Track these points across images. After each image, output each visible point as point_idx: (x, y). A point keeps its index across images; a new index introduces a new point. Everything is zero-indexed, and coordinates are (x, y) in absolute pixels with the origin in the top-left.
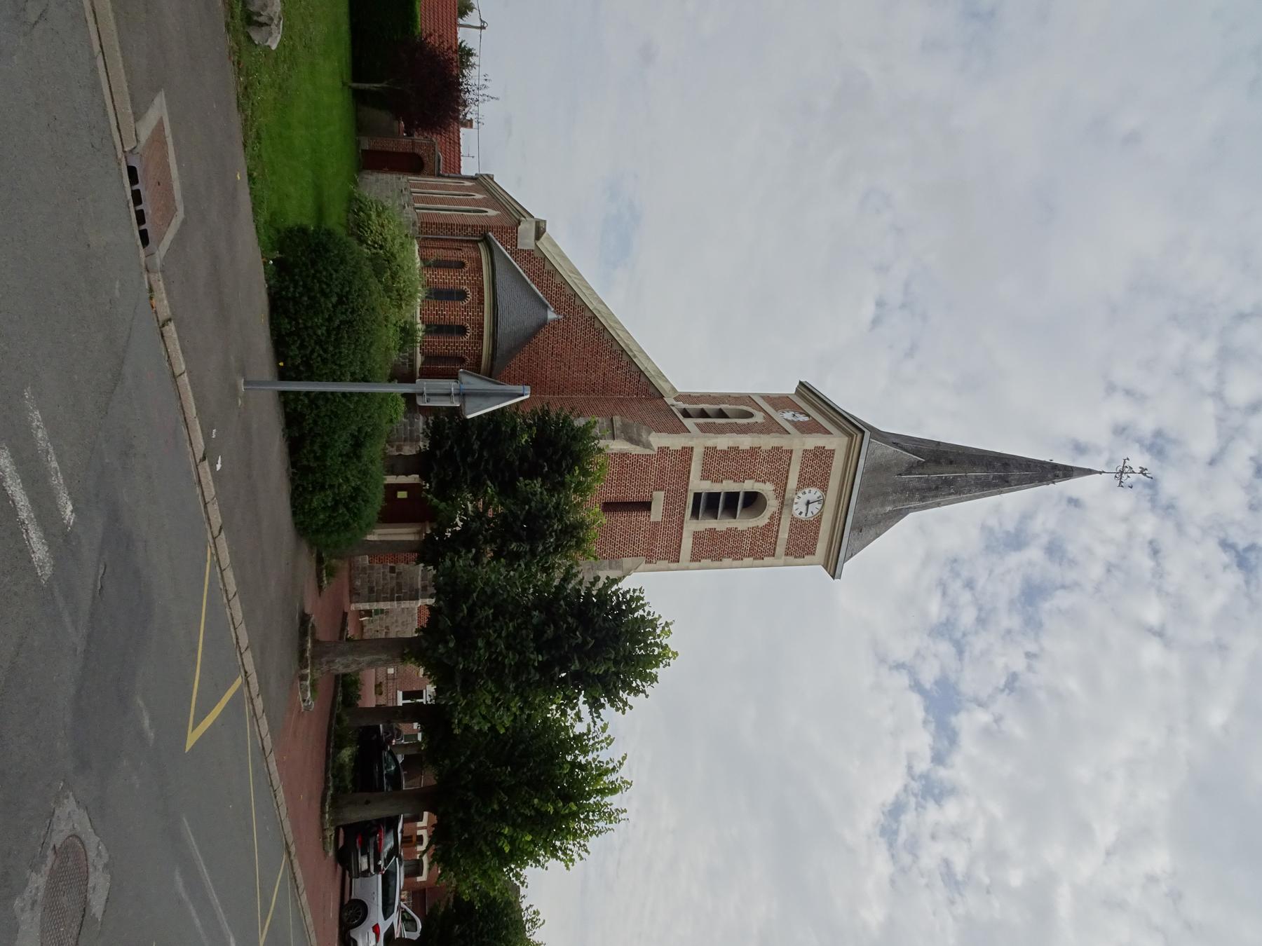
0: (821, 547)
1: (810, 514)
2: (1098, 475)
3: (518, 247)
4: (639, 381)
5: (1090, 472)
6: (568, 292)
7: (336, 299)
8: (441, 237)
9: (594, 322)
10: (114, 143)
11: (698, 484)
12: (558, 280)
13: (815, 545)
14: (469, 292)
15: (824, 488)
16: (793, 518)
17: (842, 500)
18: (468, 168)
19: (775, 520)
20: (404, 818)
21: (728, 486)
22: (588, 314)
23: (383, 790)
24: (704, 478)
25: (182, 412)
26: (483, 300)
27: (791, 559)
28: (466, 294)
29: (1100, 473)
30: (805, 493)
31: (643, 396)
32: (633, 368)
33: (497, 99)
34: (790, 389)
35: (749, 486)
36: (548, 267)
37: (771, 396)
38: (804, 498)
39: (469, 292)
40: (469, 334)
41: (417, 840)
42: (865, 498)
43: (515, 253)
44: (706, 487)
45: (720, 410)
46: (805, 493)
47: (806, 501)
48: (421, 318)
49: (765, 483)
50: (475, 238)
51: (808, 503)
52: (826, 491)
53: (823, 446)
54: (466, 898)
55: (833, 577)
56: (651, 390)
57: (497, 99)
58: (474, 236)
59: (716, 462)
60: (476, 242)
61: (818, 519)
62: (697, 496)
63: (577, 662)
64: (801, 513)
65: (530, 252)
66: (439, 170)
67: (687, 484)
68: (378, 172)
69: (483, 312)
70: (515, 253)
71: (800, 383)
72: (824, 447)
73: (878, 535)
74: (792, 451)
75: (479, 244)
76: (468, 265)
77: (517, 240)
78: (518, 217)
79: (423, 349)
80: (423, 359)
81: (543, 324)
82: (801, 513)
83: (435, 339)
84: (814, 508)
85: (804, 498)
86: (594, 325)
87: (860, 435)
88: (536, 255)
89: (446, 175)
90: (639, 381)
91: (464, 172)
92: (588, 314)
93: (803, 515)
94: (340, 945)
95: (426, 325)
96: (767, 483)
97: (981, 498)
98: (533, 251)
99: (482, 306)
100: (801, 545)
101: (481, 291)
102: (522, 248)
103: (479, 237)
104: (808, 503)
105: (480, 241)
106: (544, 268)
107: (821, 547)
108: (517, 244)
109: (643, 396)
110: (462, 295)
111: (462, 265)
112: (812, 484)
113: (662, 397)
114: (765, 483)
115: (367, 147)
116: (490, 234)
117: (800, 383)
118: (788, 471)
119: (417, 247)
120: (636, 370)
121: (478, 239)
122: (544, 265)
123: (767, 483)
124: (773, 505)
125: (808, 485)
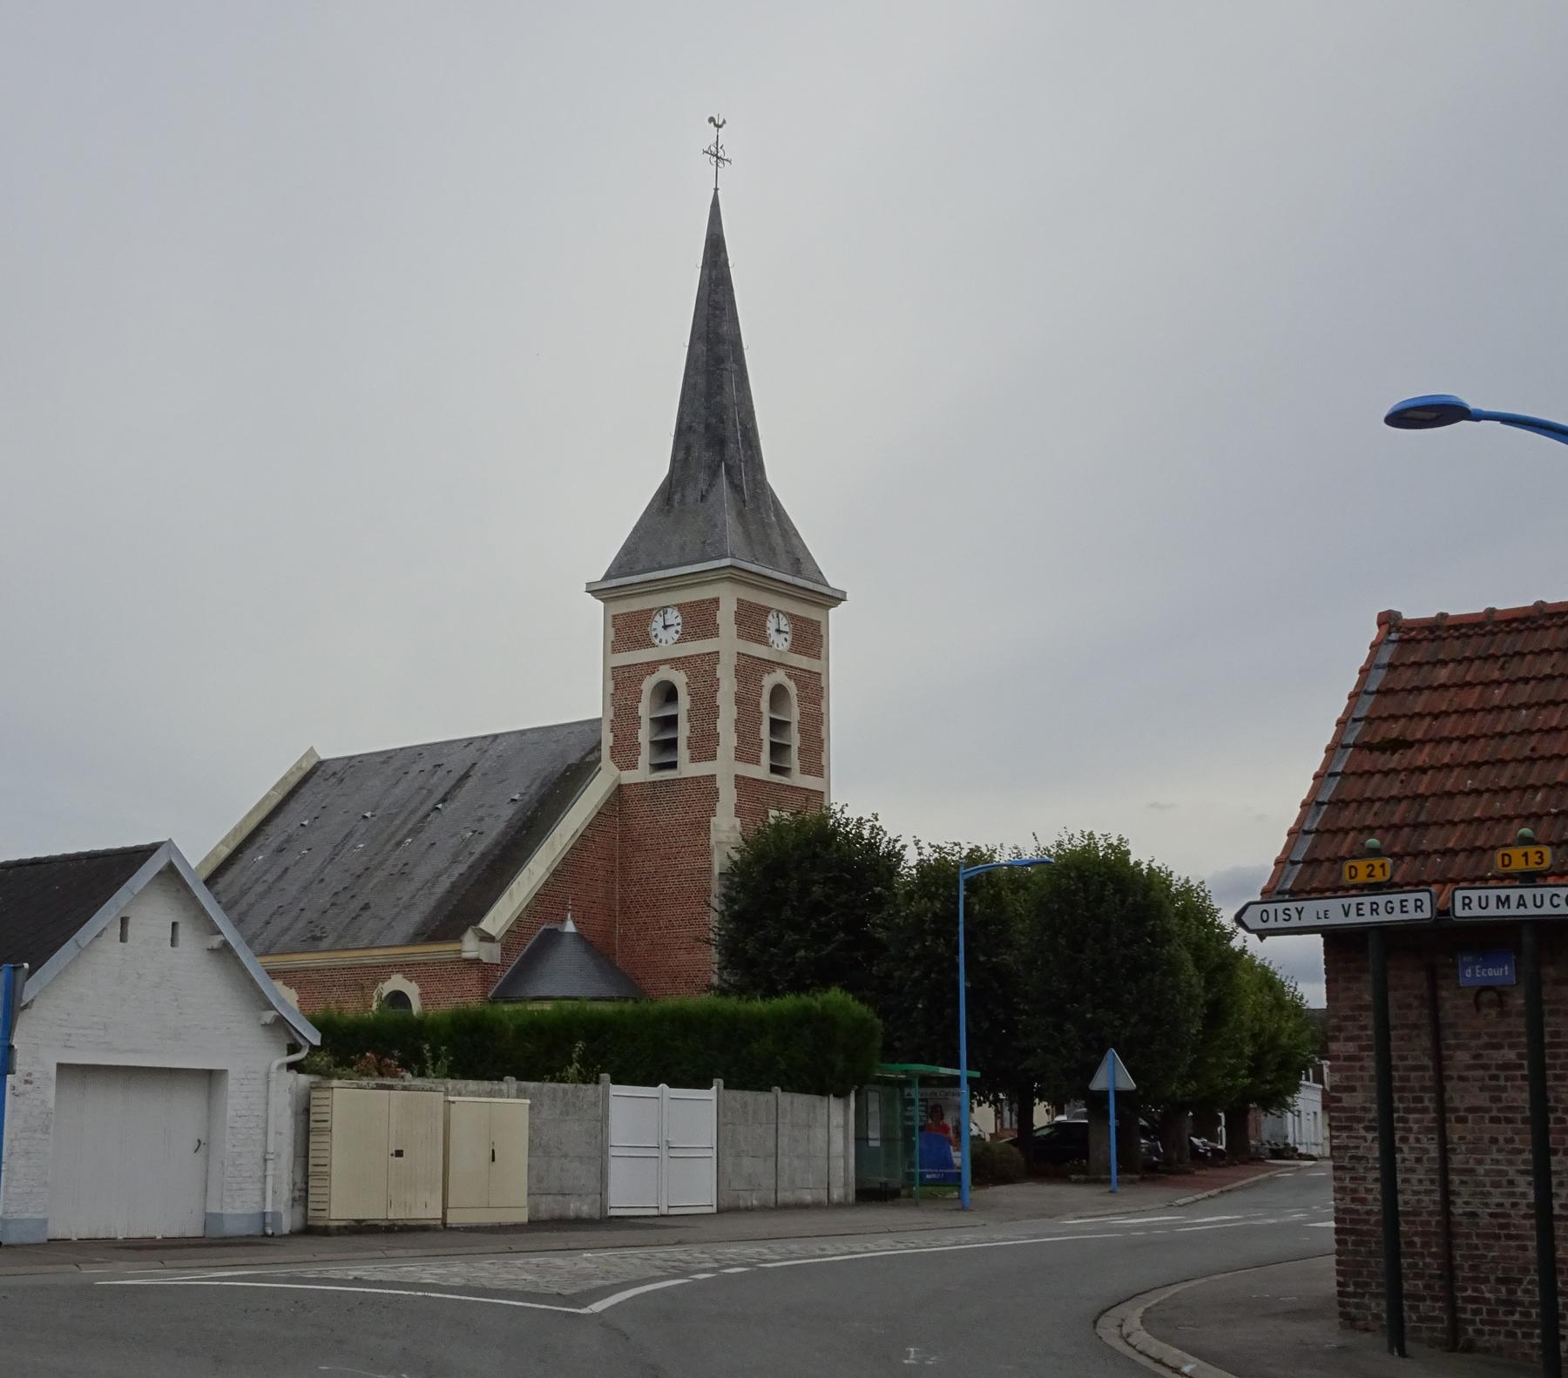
0: (811, 613)
3: (499, 962)
15: (767, 610)
16: (679, 641)
17: (780, 590)
19: (676, 663)
20: (1272, 1159)
24: (758, 762)
29: (716, 189)
42: (771, 558)
44: (645, 756)
51: (778, 631)
54: (676, 637)
59: (746, 753)
61: (792, 618)
63: (1470, 1275)
67: (763, 781)
73: (797, 534)
74: (738, 653)
81: (579, 936)
88: (505, 941)
93: (787, 637)
94: (8, 866)
100: (810, 638)
107: (811, 613)
124: (779, 676)
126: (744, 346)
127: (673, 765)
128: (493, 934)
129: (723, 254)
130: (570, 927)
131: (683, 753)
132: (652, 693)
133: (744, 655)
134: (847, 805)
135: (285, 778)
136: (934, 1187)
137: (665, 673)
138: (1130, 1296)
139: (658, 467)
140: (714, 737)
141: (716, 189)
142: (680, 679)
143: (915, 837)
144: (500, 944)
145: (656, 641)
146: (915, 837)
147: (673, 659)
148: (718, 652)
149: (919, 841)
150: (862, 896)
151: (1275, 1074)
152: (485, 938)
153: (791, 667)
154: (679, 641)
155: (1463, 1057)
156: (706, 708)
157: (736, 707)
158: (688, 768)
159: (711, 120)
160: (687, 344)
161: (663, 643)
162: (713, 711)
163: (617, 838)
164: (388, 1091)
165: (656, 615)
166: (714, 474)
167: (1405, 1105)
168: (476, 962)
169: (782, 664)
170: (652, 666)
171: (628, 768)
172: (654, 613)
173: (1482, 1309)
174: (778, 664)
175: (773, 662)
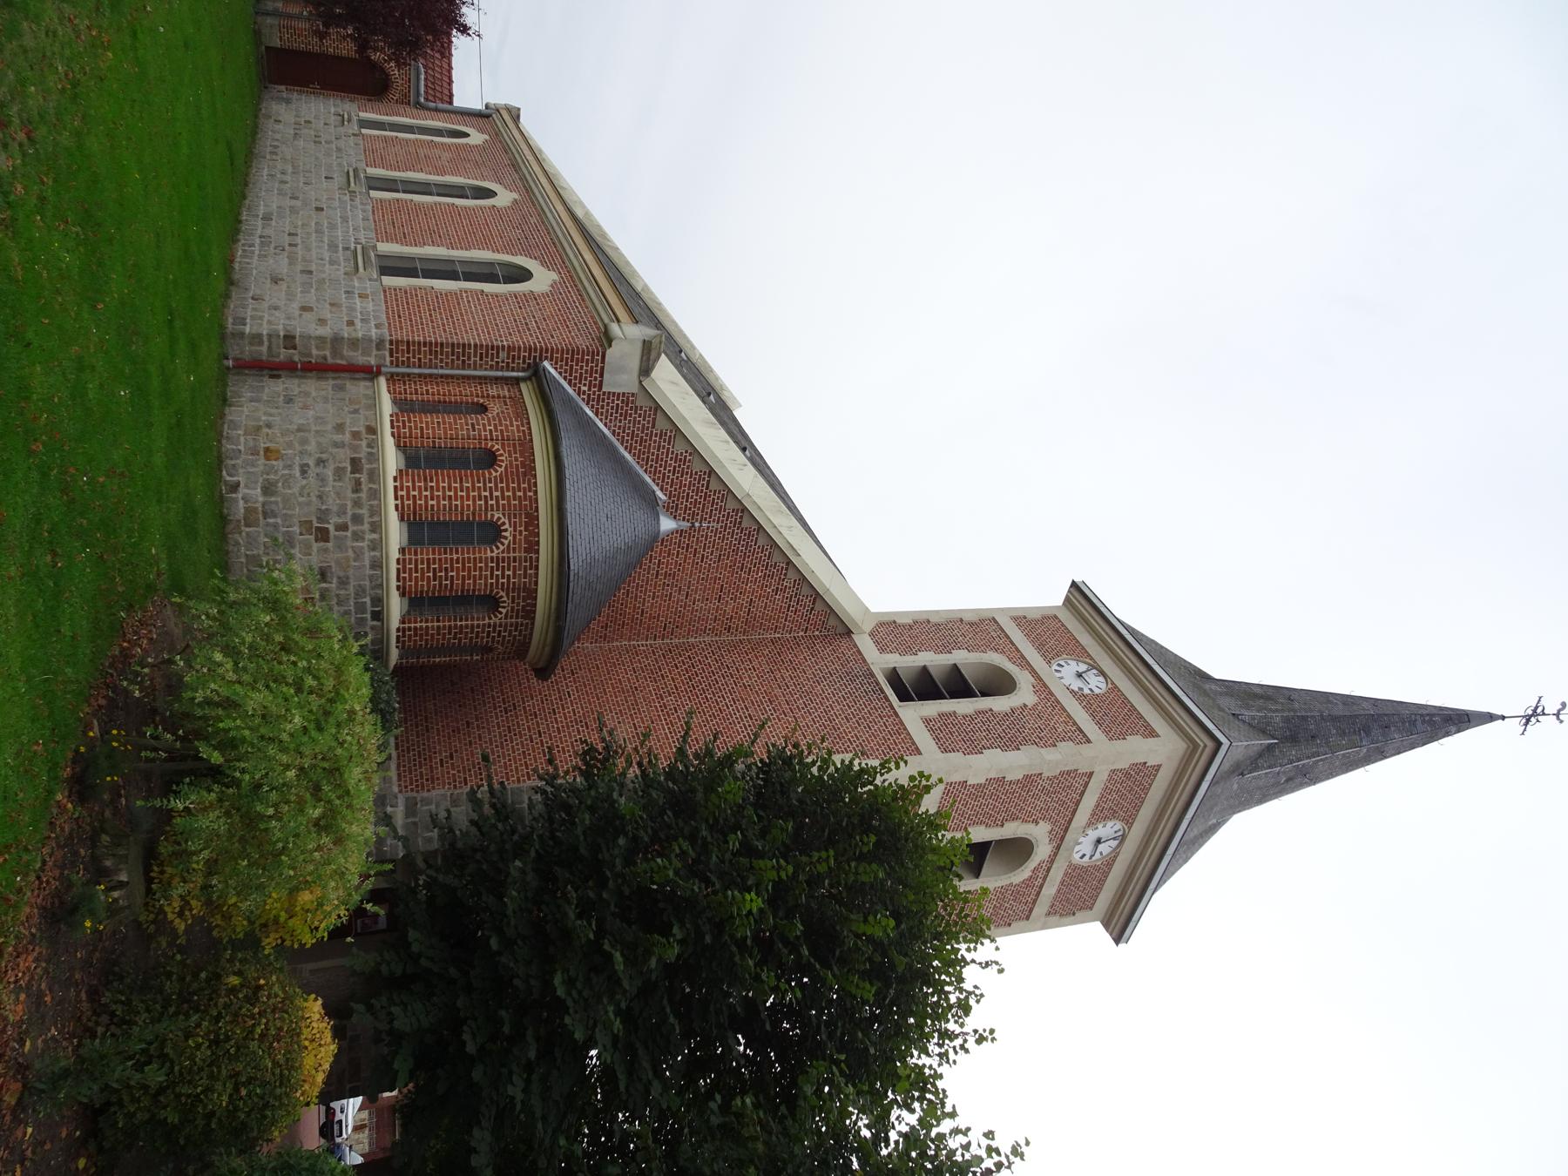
1: (1097, 856)
2: (1500, 721)
4: (812, 609)
5: (1490, 718)
6: (697, 467)
8: (441, 371)
9: (741, 517)
12: (679, 448)
13: (1095, 898)
14: (507, 526)
15: (1129, 821)
18: (468, 92)
22: (731, 505)
26: (538, 543)
27: (1055, 918)
28: (494, 453)
29: (1503, 718)
31: (817, 633)
32: (805, 590)
34: (1053, 596)
35: (1012, 830)
36: (661, 424)
37: (1029, 616)
39: (507, 526)
40: (504, 611)
41: (378, 620)
43: (599, 399)
45: (955, 668)
48: (397, 507)
49: (1037, 823)
50: (515, 374)
51: (1099, 841)
52: (1132, 824)
53: (1143, 761)
55: (1117, 940)
56: (832, 622)
58: (513, 370)
60: (517, 381)
65: (626, 398)
66: (418, 94)
68: (301, 92)
69: (537, 568)
70: (599, 399)
71: (1074, 584)
72: (1145, 763)
74: (1091, 774)
75: (523, 386)
76: (504, 458)
77: (602, 375)
78: (606, 320)
79: (404, 578)
80: (406, 607)
81: (655, 538)
83: (428, 623)
84: (1105, 848)
85: (1093, 834)
86: (740, 523)
87: (1210, 745)
89: (432, 105)
90: (812, 609)
91: (459, 101)
92: (731, 505)
93: (1086, 858)
95: (410, 598)
96: (1041, 822)
98: (633, 394)
99: (534, 556)
101: (532, 520)
102: (612, 390)
103: (524, 370)
104: (1099, 841)
105: (524, 379)
106: (653, 427)
108: (601, 382)
109: (817, 633)
110: (492, 533)
111: (490, 459)
112: (1113, 815)
113: (849, 632)
114: (1037, 823)
115: (277, 43)
116: (546, 364)
117: (1074, 584)
118: (1078, 803)
119: (387, 407)
120: (809, 592)
121: (521, 374)
122: (654, 420)
123: (1041, 822)
124: (1042, 851)
126: (1367, 767)
128: (654, 374)
129: (1453, 729)
130: (667, 524)
132: (987, 664)
133: (1087, 784)
134: (1001, 971)
135: (712, 371)
137: (1023, 678)
139: (1222, 666)
140: (974, 747)
141: (1503, 718)
142: (1024, 695)
143: (1028, 1143)
144: (635, 389)
145: (1055, 667)
146: (1028, 1143)
147: (1045, 685)
149: (1022, 1156)
152: (649, 351)
153: (1048, 870)
156: (1010, 734)
157: (1021, 777)
159: (1564, 705)
160: (1353, 694)
162: (1011, 742)
163: (777, 635)
165: (1085, 663)
166: (1264, 732)
167: (374, 349)
168: (607, 339)
169: (1056, 854)
171: (877, 643)
172: (1088, 660)
174: (1058, 848)
175: (1062, 839)
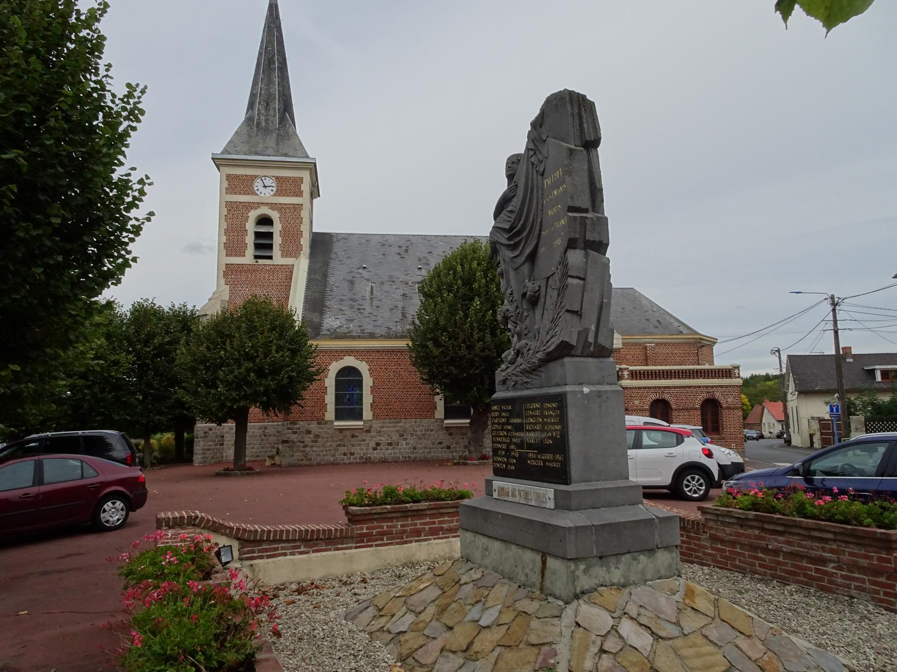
1: (274, 185)
7: (84, 370)
10: (232, 154)
11: (248, 258)
16: (275, 195)
19: (272, 206)
21: (250, 239)
23: (568, 211)
25: (634, 650)
30: (258, 190)
33: (786, 29)
38: (262, 189)
44: (250, 251)
46: (258, 190)
47: (264, 188)
51: (265, 187)
54: (272, 193)
57: (786, 29)
61: (278, 178)
62: (256, 257)
64: (272, 190)
82: (272, 190)
93: (273, 188)
97: (255, 71)
104: (265, 187)
123: (249, 215)
125: (252, 182)
127: (271, 258)
131: (276, 252)
136: (521, 200)
138: (536, 508)
142: (275, 215)
145: (258, 193)
148: (302, 205)
150: (54, 59)
151: (62, 316)
154: (275, 195)
155: (637, 402)
158: (278, 258)
161: (263, 195)
164: (715, 358)
170: (258, 205)
173: (824, 578)
